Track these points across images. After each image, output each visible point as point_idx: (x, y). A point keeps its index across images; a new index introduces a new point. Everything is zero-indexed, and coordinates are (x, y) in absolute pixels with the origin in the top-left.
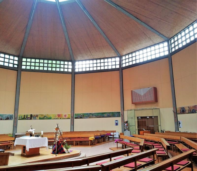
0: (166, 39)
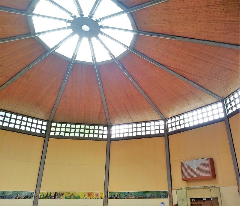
0: (220, 99)
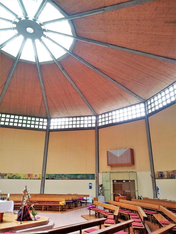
0: (143, 100)
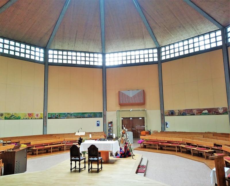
0: (158, 46)
